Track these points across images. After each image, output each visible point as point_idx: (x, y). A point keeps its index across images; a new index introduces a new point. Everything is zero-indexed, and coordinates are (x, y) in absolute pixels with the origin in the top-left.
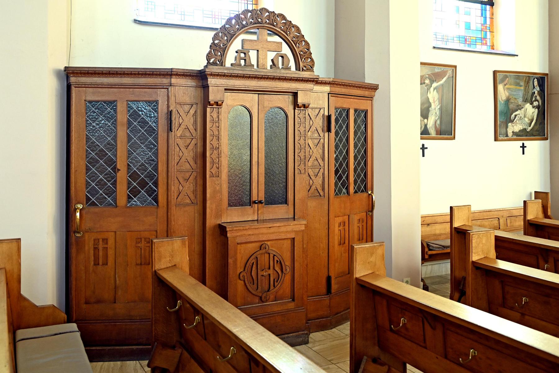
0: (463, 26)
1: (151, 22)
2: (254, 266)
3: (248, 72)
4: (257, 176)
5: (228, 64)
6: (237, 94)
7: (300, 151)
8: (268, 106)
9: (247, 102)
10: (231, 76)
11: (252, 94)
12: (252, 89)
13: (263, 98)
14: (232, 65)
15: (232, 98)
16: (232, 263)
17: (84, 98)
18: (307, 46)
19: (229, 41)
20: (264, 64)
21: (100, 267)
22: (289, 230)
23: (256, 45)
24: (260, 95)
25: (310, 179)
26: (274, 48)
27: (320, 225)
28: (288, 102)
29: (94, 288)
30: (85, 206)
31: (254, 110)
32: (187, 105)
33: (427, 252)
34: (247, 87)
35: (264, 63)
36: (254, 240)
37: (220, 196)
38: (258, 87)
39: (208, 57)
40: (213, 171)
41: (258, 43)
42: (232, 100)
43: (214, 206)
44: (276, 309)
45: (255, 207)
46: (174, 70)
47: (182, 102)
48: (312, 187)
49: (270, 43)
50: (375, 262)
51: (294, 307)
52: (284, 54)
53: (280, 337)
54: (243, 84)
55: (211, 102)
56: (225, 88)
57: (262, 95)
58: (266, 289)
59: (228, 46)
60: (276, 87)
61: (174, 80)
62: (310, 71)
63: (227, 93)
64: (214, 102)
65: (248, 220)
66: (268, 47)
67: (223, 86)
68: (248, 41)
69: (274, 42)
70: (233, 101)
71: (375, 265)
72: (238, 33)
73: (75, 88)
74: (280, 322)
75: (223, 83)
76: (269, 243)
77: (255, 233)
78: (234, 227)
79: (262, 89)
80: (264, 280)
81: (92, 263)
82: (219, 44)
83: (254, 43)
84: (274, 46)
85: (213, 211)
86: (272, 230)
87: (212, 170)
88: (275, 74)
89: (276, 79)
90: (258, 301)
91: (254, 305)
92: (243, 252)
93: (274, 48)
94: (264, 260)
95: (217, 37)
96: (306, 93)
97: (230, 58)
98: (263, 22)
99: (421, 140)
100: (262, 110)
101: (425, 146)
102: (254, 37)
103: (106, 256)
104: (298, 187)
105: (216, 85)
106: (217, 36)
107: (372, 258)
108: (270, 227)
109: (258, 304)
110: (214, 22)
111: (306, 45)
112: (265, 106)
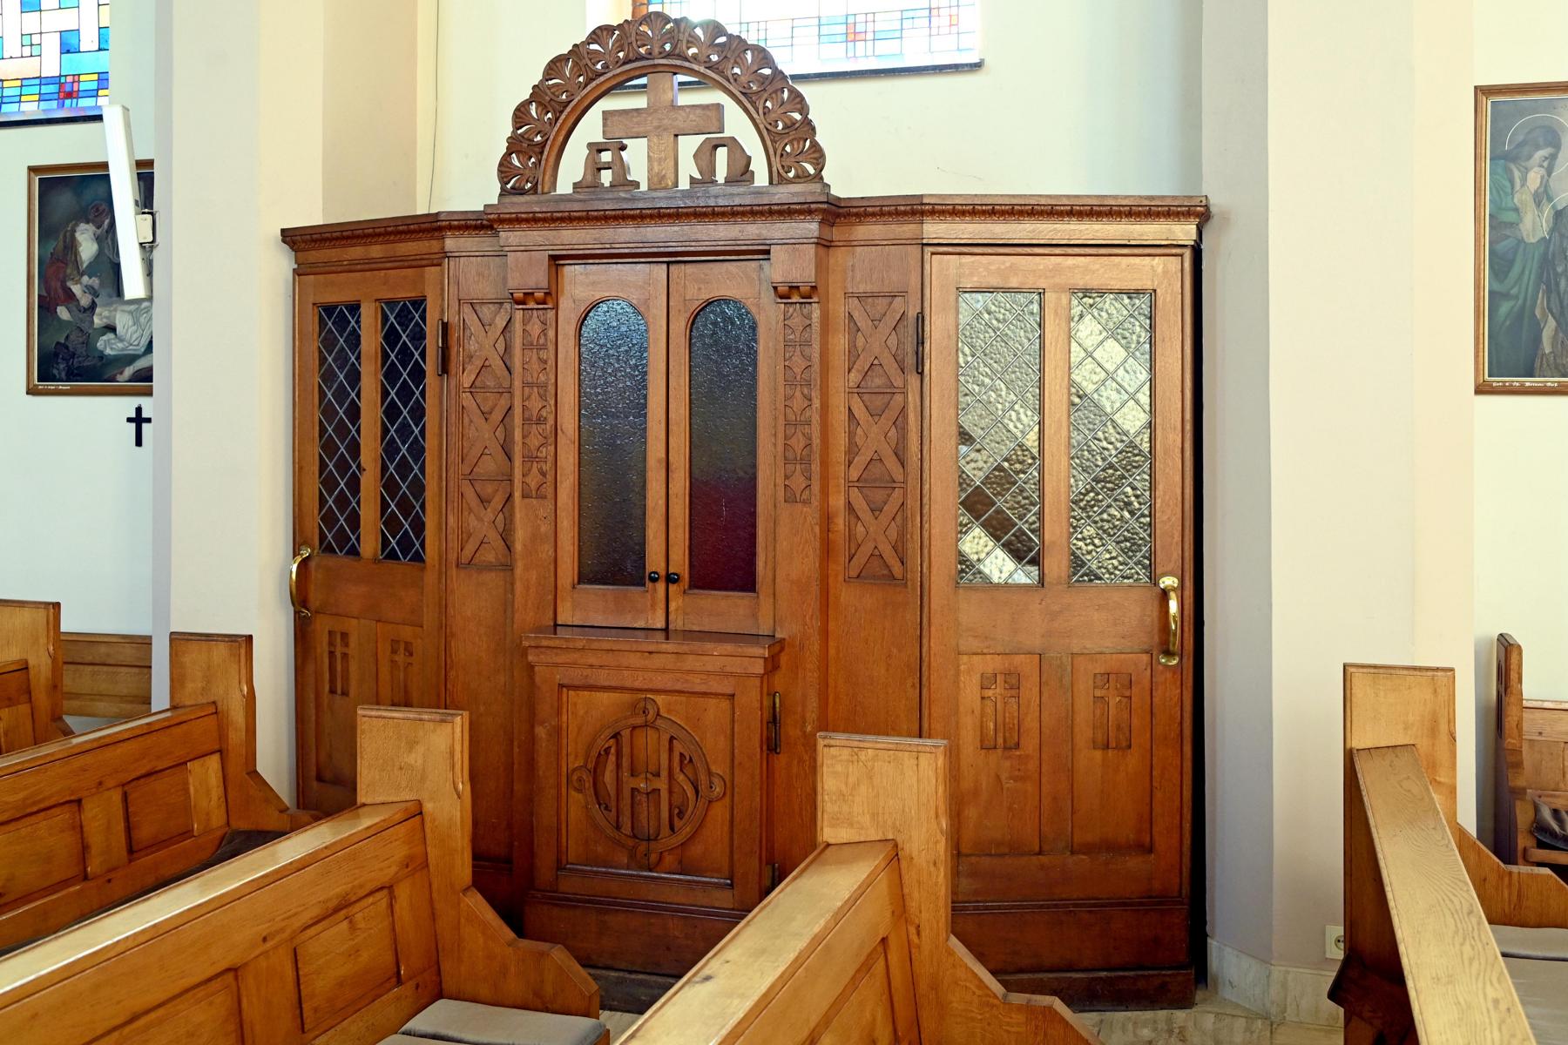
0: (52, 45)
1: (859, 71)
2: (612, 758)
3: (739, 197)
4: (662, 502)
5: (564, 186)
6: (604, 266)
7: (793, 431)
8: (695, 298)
9: (632, 290)
10: (554, 220)
11: (648, 265)
12: (627, 251)
13: (682, 275)
14: (576, 186)
15: (587, 281)
16: (544, 736)
17: (311, 300)
18: (798, 103)
19: (556, 123)
20: (664, 176)
21: (338, 697)
22: (710, 668)
23: (638, 124)
24: (672, 268)
25: (856, 520)
26: (694, 123)
27: (887, 670)
28: (757, 282)
29: (331, 746)
30: (316, 551)
31: (655, 311)
32: (491, 306)
33: (1525, 850)
34: (608, 246)
35: (664, 172)
36: (606, 684)
37: (548, 551)
38: (641, 245)
39: (505, 170)
40: (532, 481)
41: (644, 115)
42: (588, 286)
43: (534, 577)
44: (678, 897)
45: (655, 590)
46: (442, 217)
47: (475, 297)
48: (862, 548)
49: (680, 112)
50: (424, 770)
51: (731, 907)
52: (730, 138)
53: (593, 971)
54: (595, 239)
55: (779, 288)
56: (551, 253)
57: (680, 265)
58: (651, 832)
59: (552, 137)
60: (693, 238)
61: (450, 243)
62: (806, 179)
63: (573, 266)
64: (790, 287)
65: (636, 625)
66: (675, 123)
67: (541, 248)
68: (615, 115)
69: (693, 106)
70: (590, 288)
71: (423, 779)
72: (579, 98)
73: (301, 277)
74: (678, 938)
75: (540, 240)
76: (660, 699)
77: (606, 664)
78: (543, 638)
79: (655, 250)
80: (645, 805)
81: (327, 688)
82: (526, 136)
83: (633, 117)
84: (694, 118)
85: (531, 591)
86: (658, 661)
87: (528, 480)
88: (680, 202)
89: (558, 219)
90: (626, 861)
91: (613, 870)
92: (581, 712)
93: (694, 123)
94: (650, 745)
95: (524, 116)
96: (798, 250)
97: (571, 169)
98: (653, 54)
99: (30, 397)
100: (679, 311)
101: (145, 415)
102: (640, 102)
103: (346, 678)
104: (785, 543)
105: (522, 248)
106: (522, 113)
107: (413, 755)
108: (650, 653)
109: (628, 869)
110: (851, 54)
111: (794, 100)
112: (687, 298)
